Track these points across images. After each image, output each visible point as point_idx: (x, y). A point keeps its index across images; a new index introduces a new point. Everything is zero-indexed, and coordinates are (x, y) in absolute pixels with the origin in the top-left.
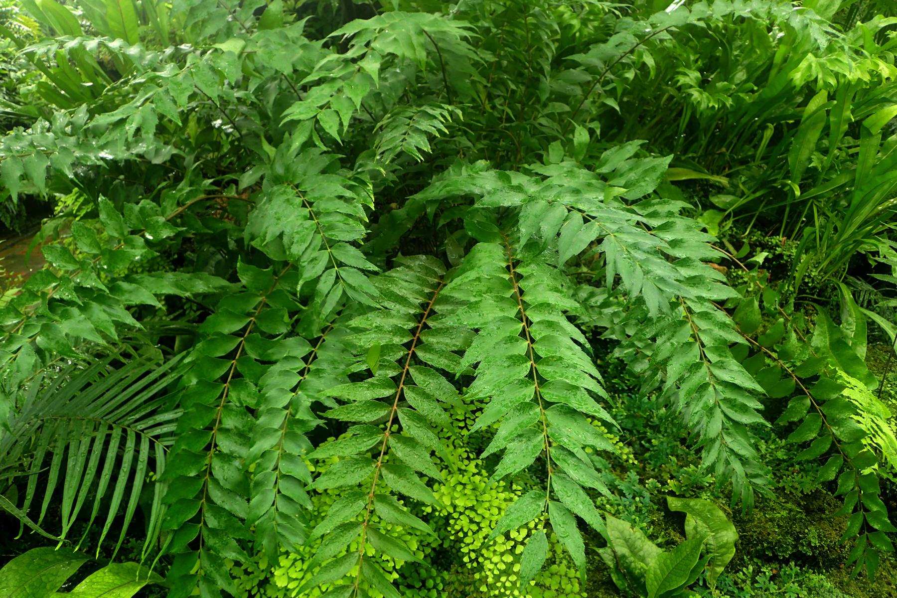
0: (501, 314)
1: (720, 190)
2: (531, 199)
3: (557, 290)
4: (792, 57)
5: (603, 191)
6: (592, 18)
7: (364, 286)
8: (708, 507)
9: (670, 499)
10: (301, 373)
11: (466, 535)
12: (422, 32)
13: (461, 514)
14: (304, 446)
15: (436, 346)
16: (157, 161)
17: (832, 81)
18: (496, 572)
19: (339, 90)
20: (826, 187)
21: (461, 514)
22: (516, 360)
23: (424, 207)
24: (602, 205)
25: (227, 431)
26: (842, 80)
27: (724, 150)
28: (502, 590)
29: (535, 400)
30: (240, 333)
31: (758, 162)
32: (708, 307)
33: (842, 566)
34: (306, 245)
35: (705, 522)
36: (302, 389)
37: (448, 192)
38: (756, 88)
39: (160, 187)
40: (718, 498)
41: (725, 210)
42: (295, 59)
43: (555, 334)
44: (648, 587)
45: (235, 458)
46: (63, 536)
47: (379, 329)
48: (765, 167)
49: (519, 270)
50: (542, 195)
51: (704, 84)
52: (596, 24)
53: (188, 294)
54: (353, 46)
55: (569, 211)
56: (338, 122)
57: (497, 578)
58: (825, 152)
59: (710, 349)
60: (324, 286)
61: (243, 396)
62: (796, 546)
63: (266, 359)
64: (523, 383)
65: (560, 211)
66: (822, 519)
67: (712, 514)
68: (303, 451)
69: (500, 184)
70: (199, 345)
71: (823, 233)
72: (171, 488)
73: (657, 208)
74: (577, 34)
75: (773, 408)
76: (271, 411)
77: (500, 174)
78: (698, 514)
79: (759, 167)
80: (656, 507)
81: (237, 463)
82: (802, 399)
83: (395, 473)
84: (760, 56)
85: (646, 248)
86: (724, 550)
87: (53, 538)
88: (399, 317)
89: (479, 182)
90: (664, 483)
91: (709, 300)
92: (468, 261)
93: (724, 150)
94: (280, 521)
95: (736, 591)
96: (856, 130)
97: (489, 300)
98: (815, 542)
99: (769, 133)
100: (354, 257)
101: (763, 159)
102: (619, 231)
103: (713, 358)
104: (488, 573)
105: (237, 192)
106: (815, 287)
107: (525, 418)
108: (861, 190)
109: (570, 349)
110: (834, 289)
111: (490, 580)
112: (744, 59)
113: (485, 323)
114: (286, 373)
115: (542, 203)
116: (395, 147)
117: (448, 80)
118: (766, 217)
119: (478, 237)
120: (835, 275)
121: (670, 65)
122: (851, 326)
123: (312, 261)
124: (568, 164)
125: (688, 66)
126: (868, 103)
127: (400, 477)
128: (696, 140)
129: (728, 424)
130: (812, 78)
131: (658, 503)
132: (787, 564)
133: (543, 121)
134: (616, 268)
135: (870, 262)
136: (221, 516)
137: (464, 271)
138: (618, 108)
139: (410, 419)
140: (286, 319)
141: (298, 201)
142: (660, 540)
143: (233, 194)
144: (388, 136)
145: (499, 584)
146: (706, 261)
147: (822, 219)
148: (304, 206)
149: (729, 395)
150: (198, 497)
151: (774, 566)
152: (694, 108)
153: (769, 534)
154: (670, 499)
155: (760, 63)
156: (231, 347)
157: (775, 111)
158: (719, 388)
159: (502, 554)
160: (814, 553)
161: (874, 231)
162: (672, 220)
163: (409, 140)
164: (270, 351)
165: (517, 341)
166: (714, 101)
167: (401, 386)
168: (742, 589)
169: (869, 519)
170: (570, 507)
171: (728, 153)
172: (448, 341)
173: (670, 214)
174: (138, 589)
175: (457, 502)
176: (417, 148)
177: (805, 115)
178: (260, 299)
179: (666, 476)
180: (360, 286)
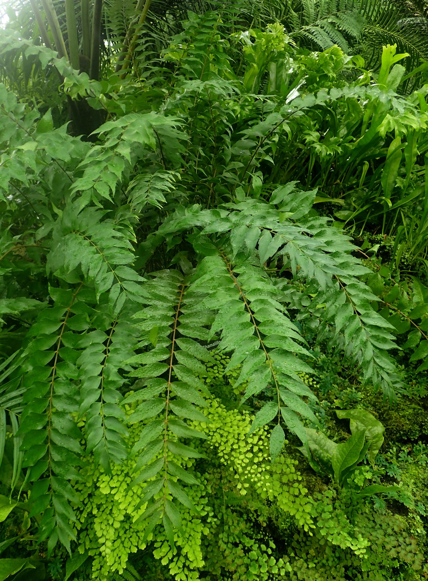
1: (340, 208)
2: (236, 225)
5: (278, 216)
6: (247, 104)
7: (139, 291)
9: (337, 412)
10: (105, 352)
11: (220, 444)
12: (151, 126)
13: (214, 432)
14: (117, 398)
15: (191, 325)
17: (404, 131)
18: (244, 465)
19: (106, 168)
21: (214, 432)
22: (244, 326)
23: (164, 239)
24: (280, 224)
25: (60, 396)
26: (410, 130)
27: (338, 181)
28: (249, 475)
29: (261, 348)
30: (58, 332)
31: (361, 187)
35: (362, 423)
36: (108, 362)
37: (180, 226)
38: (355, 139)
40: (368, 407)
41: (344, 221)
42: (70, 150)
43: (266, 306)
44: (334, 468)
45: (67, 413)
47: (153, 318)
48: (367, 190)
49: (235, 271)
50: (242, 222)
51: (321, 139)
52: (250, 107)
53: (16, 312)
54: (108, 139)
56: (108, 189)
57: (244, 468)
58: (404, 176)
59: (359, 306)
60: (113, 295)
61: (67, 373)
62: (421, 431)
63: (79, 347)
64: (251, 339)
65: (256, 231)
67: (366, 417)
68: (117, 401)
69: (214, 218)
70: (30, 344)
71: (409, 229)
72: (25, 441)
73: (312, 223)
74: (239, 116)
75: (401, 340)
76: (91, 379)
77: (213, 211)
79: (363, 189)
80: (330, 418)
81: (68, 417)
82: (416, 332)
83: (179, 406)
85: (313, 248)
86: (377, 439)
88: (162, 309)
89: (201, 218)
90: (332, 402)
92: (201, 269)
93: (338, 181)
94: (109, 446)
95: (388, 465)
97: (221, 291)
99: (366, 168)
100: (131, 274)
101: (364, 185)
104: (239, 466)
106: (409, 265)
107: (256, 360)
109: (277, 314)
110: (421, 264)
111: (240, 470)
112: (345, 120)
113: (222, 306)
114: (95, 354)
115: (244, 227)
116: (143, 202)
117: (164, 154)
118: (372, 224)
120: (420, 255)
121: (299, 128)
123: (103, 279)
124: (251, 201)
125: (310, 129)
127: (182, 407)
128: (320, 176)
129: (377, 351)
130: (392, 130)
131: (330, 415)
132: (417, 443)
133: (228, 175)
136: (62, 453)
137: (199, 277)
138: (273, 162)
140: (88, 319)
141: (87, 242)
142: (335, 439)
143: (32, 243)
144: (136, 194)
145: (246, 472)
147: (407, 220)
148: (91, 245)
149: (374, 333)
150: (46, 443)
151: (408, 446)
152: (318, 157)
153: (403, 425)
154: (337, 412)
156: (52, 343)
157: (369, 153)
158: (368, 329)
159: (245, 453)
162: (323, 229)
163: (151, 196)
164: (80, 342)
165: (243, 314)
166: (330, 150)
167: (173, 352)
168: (391, 463)
170: (294, 409)
172: (197, 320)
173: (321, 226)
174: (11, 509)
175: (210, 425)
176: (158, 201)
177: (389, 154)
178: (66, 309)
179: (333, 397)
180: (137, 292)
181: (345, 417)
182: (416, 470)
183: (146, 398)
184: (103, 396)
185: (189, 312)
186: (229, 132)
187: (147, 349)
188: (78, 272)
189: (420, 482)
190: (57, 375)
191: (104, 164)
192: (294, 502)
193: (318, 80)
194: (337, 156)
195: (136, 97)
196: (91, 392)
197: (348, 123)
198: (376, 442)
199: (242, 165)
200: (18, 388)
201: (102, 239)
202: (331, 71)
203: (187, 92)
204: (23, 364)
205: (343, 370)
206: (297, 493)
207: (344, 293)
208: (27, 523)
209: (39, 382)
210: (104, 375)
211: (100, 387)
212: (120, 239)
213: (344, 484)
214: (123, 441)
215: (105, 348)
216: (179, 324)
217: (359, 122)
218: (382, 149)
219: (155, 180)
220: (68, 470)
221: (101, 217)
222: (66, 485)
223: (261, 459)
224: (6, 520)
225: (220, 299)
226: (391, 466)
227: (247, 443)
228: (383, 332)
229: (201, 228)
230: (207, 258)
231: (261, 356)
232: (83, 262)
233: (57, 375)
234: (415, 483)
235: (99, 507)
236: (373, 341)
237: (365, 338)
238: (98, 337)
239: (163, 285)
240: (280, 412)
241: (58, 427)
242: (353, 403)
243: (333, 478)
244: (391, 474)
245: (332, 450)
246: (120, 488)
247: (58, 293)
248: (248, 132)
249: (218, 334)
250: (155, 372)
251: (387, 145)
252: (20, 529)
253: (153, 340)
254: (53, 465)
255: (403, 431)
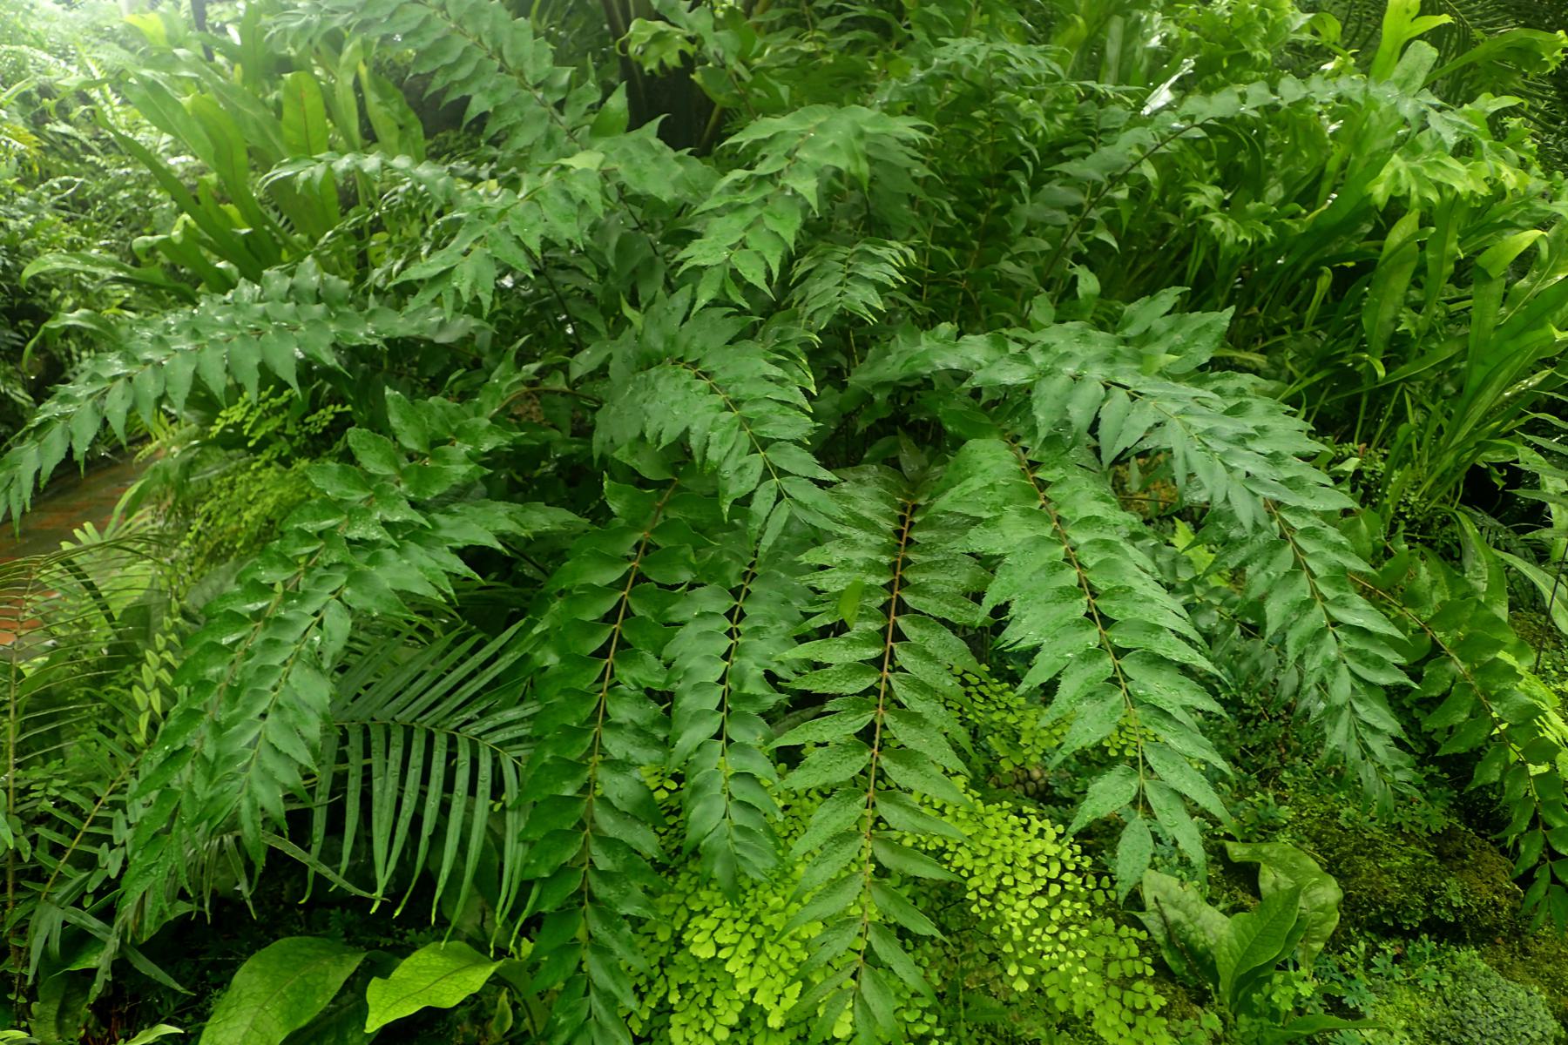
0: (1032, 534)
2: (1046, 373)
3: (1104, 499)
4: (1355, 163)
6: (1060, 107)
8: (1290, 854)
9: (1229, 845)
10: (730, 634)
11: (971, 874)
12: (861, 135)
14: (760, 733)
15: (932, 588)
16: (442, 339)
17: (1434, 197)
18: (1026, 923)
20: (1425, 363)
22: (1065, 594)
25: (619, 726)
27: (1255, 310)
30: (621, 584)
32: (1312, 522)
33: (1499, 940)
34: (729, 446)
35: (1288, 875)
36: (738, 654)
39: (452, 378)
40: (1302, 842)
42: (673, 177)
43: (1112, 556)
44: (1220, 968)
45: (633, 765)
46: (379, 893)
47: (846, 564)
48: (1324, 336)
52: (1067, 116)
54: (764, 157)
55: (1107, 388)
57: (1027, 931)
58: (1417, 308)
59: (1323, 580)
60: (760, 506)
62: (1428, 909)
65: (1092, 390)
66: (1464, 866)
69: (994, 354)
70: (556, 605)
71: (1421, 436)
76: (699, 688)
78: (1276, 864)
81: (635, 774)
84: (1307, 162)
87: (366, 894)
91: (1314, 512)
92: (957, 468)
93: (1255, 310)
94: (737, 838)
96: (1464, 274)
97: (1012, 514)
98: (1458, 901)
99: (1325, 282)
100: (803, 463)
101: (1315, 323)
102: (1184, 412)
103: (1329, 593)
104: (1014, 924)
105: (567, 381)
106: (1415, 521)
108: (1484, 363)
109: (1139, 577)
110: (1447, 522)
111: (1017, 933)
114: (709, 635)
116: (831, 305)
119: (964, 433)
120: (1444, 501)
122: (1480, 573)
123: (740, 469)
125: (1201, 180)
126: (1481, 230)
134: (1187, 465)
135: (1496, 481)
138: (1115, 245)
139: (910, 689)
141: (703, 384)
142: (1222, 906)
144: (815, 287)
146: (1307, 458)
148: (712, 391)
152: (1215, 248)
153: (1386, 892)
154: (1229, 845)
155: (1304, 171)
156: (608, 605)
160: (1457, 918)
161: (1504, 429)
164: (670, 609)
165: (1062, 568)
168: (1352, 977)
169: (1551, 841)
171: (1261, 315)
173: (1240, 392)
174: (492, 969)
177: (1381, 259)
181: (1247, 859)
182: (1411, 998)
183: (826, 738)
184: (727, 726)
185: (929, 559)
186: (1029, 164)
187: (840, 628)
188: (681, 453)
189: (1421, 1027)
190: (616, 679)
191: (751, 214)
192: (1131, 1026)
193: (1225, 65)
194: (1257, 250)
195: (805, 74)
196: (699, 716)
197: (1288, 174)
198: (1321, 922)
199: (1046, 246)
200: (517, 705)
201: (738, 379)
202: (1259, 44)
203: (939, 66)
204: (535, 649)
205: (1244, 754)
206: (1140, 1006)
207: (1290, 547)
208: (503, 1018)
209: (575, 691)
210: (729, 683)
211: (720, 708)
212: (780, 382)
213: (1242, 1005)
214: (770, 831)
215: (730, 625)
216: (904, 583)
217: (1316, 173)
218: (1364, 244)
219: (860, 259)
220: (627, 894)
221: (732, 332)
222: (619, 927)
223: (1068, 913)
224: (456, 1007)
225: (1007, 532)
226: (1353, 984)
227: (1035, 877)
228: (1376, 646)
229: (960, 376)
230: (972, 444)
231: (1101, 664)
232: (694, 428)
233: (616, 679)
234: (1408, 1030)
235: (683, 988)
236: (1351, 663)
237: (1333, 654)
238: (712, 600)
239: (866, 495)
240: (1141, 789)
241: (612, 796)
242: (1266, 829)
243: (1217, 991)
244: (1350, 1001)
245: (1215, 928)
246: (740, 948)
247: (625, 497)
248: (1073, 168)
249: (1000, 610)
250: (850, 684)
251: (1380, 233)
252: (485, 1033)
253: (847, 613)
254: (593, 879)
255: (1386, 905)
